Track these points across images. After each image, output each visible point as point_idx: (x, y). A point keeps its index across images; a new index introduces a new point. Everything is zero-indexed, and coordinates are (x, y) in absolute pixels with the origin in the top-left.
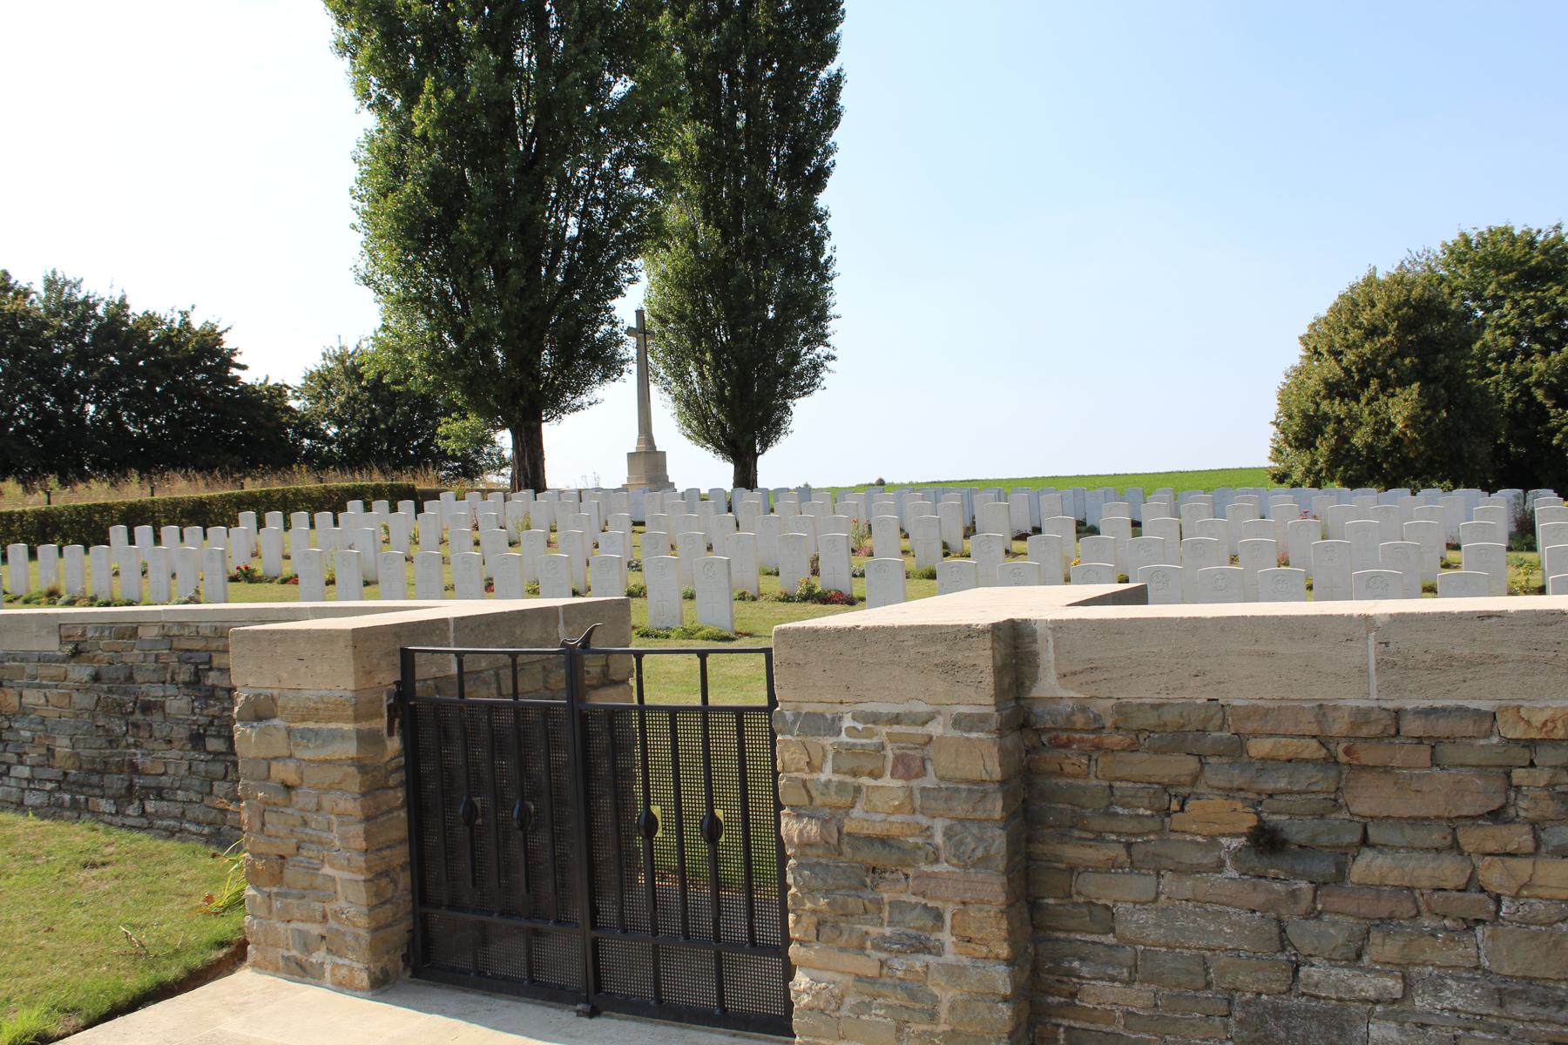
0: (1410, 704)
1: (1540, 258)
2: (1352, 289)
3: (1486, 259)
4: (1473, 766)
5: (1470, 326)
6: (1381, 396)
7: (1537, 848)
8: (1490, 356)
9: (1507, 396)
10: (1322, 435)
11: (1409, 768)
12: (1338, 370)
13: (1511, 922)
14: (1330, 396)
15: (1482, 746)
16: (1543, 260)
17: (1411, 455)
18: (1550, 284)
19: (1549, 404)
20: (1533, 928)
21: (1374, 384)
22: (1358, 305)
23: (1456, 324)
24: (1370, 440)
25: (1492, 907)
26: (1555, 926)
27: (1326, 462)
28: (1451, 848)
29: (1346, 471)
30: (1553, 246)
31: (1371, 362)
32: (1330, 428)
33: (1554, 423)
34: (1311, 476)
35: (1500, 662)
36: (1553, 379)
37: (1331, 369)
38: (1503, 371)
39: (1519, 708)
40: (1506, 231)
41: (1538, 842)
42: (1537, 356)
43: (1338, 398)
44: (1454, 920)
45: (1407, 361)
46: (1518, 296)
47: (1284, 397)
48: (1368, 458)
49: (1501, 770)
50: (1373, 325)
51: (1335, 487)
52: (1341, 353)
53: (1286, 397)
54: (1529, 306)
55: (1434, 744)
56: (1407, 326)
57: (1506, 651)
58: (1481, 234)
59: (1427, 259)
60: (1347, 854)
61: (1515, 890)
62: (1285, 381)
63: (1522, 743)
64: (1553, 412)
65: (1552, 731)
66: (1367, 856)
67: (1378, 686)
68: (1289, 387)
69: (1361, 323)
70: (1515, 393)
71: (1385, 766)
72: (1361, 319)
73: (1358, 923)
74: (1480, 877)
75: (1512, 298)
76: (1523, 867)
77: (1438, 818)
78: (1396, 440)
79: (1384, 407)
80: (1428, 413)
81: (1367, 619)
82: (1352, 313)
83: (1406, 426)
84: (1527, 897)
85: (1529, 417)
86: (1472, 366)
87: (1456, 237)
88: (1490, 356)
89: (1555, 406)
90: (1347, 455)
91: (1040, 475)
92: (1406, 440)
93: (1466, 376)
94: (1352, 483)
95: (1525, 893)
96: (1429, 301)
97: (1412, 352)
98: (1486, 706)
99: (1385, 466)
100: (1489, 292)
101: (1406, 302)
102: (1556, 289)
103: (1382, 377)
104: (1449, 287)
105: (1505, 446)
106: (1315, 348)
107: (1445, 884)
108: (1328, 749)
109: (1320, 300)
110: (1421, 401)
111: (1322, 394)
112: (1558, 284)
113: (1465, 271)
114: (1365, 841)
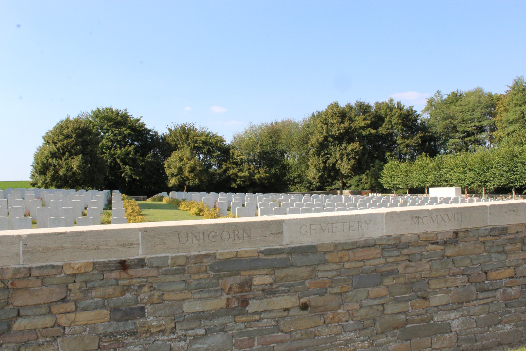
0: (34, 265)
1: (120, 118)
2: (61, 122)
3: (104, 117)
4: (56, 284)
5: (99, 138)
6: (69, 158)
7: (76, 309)
8: (105, 147)
9: (109, 161)
10: (49, 170)
11: (35, 287)
12: (55, 149)
13: (69, 335)
14: (52, 158)
15: (59, 277)
16: (121, 119)
17: (78, 178)
18: (123, 127)
19: (121, 164)
20: (75, 335)
21: (67, 154)
22: (63, 128)
23: (94, 137)
24: (65, 173)
25: (62, 331)
26: (82, 334)
27: (50, 180)
28: (49, 313)
29: (57, 183)
30: (124, 116)
31: (66, 147)
32: (52, 168)
33: (122, 170)
34: (45, 184)
35: (64, 249)
36: (122, 156)
37: (53, 148)
38: (108, 153)
39: (70, 264)
40: (111, 109)
41: (76, 308)
42: (118, 149)
43: (55, 158)
44: (50, 338)
45: (78, 147)
46: (113, 129)
47: (36, 157)
48: (64, 179)
49: (65, 285)
50: (68, 135)
51: (53, 188)
52: (56, 143)
53: (37, 157)
54: (116, 133)
55: (42, 279)
56: (79, 136)
57: (66, 245)
58: (103, 109)
59: (87, 115)
60: (12, 321)
61: (69, 324)
62: (37, 151)
63: (71, 275)
64: (122, 166)
65: (80, 270)
66: (20, 320)
67: (23, 260)
68: (38, 153)
69: (64, 134)
70: (111, 160)
71: (26, 288)
72: (64, 132)
73: (16, 345)
74: (59, 322)
75: (112, 130)
76: (72, 316)
77: (44, 303)
78: (74, 173)
79: (70, 162)
80: (84, 165)
81: (19, 237)
82: (61, 130)
83: (77, 169)
84: (73, 326)
85: (115, 168)
86: (99, 151)
87: (96, 109)
88: (105, 147)
89: (123, 165)
90: (57, 178)
91: (4, 181)
92: (77, 173)
93: (96, 153)
94: (58, 187)
95: (73, 324)
96: (86, 128)
97: (80, 144)
98: (60, 264)
99: (70, 181)
100: (104, 128)
101: (79, 128)
102: (124, 129)
103: (70, 152)
104: (93, 124)
105: (108, 176)
106: (48, 141)
107: (47, 326)
108: (5, 284)
109: (50, 125)
110: (82, 161)
111: (49, 156)
112: (125, 127)
113: (98, 120)
114: (19, 315)
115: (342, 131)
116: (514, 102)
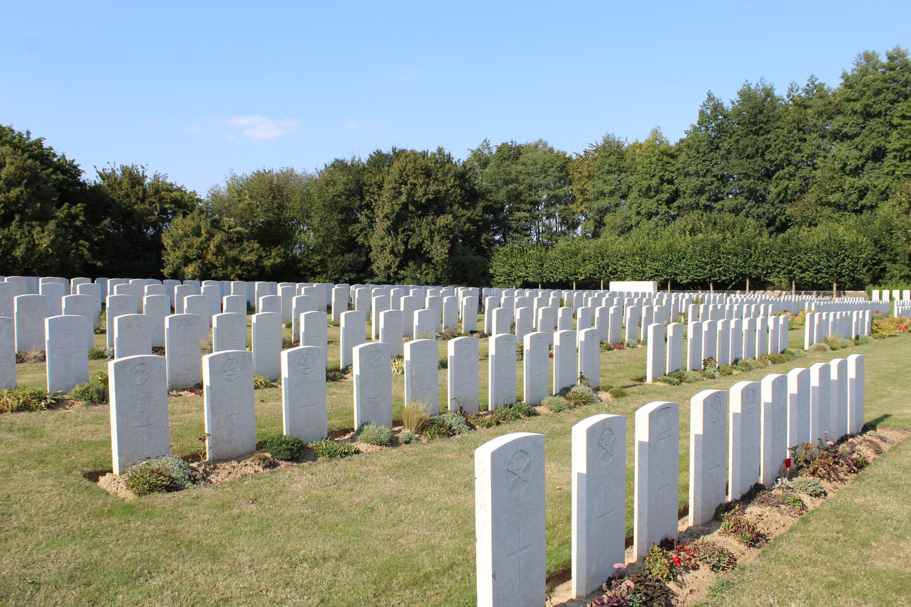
115: (431, 197)
116: (606, 167)
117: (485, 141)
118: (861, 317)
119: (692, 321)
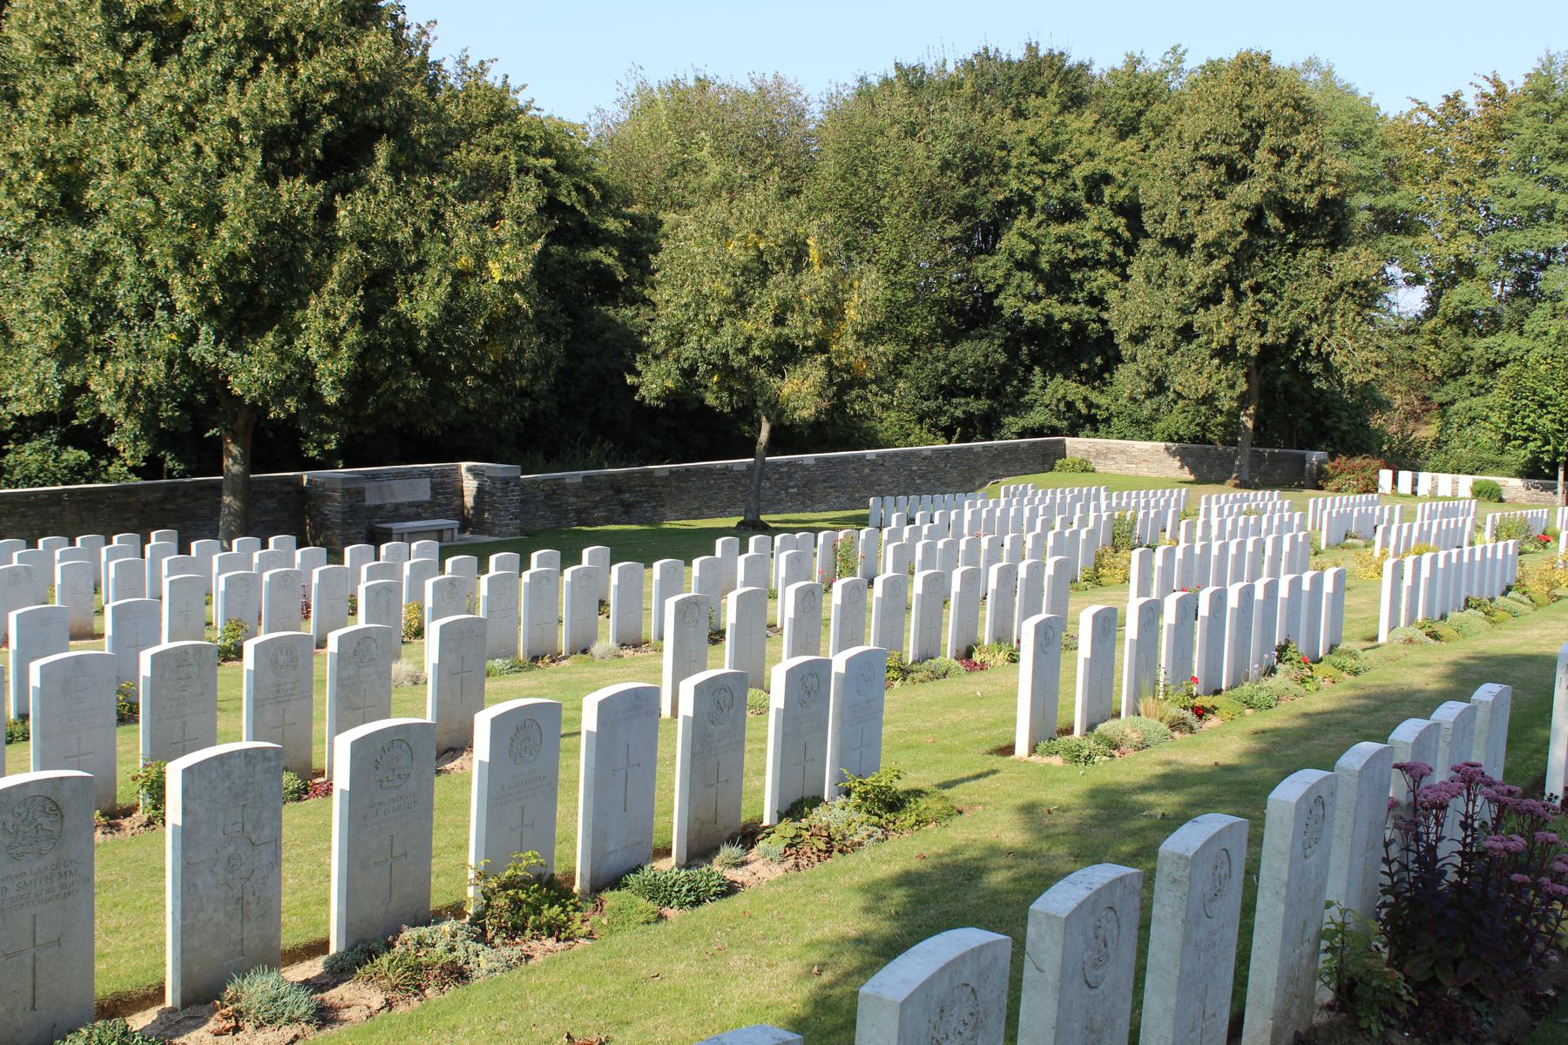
117: (1174, 50)
118: (1404, 533)
119: (1139, 596)
